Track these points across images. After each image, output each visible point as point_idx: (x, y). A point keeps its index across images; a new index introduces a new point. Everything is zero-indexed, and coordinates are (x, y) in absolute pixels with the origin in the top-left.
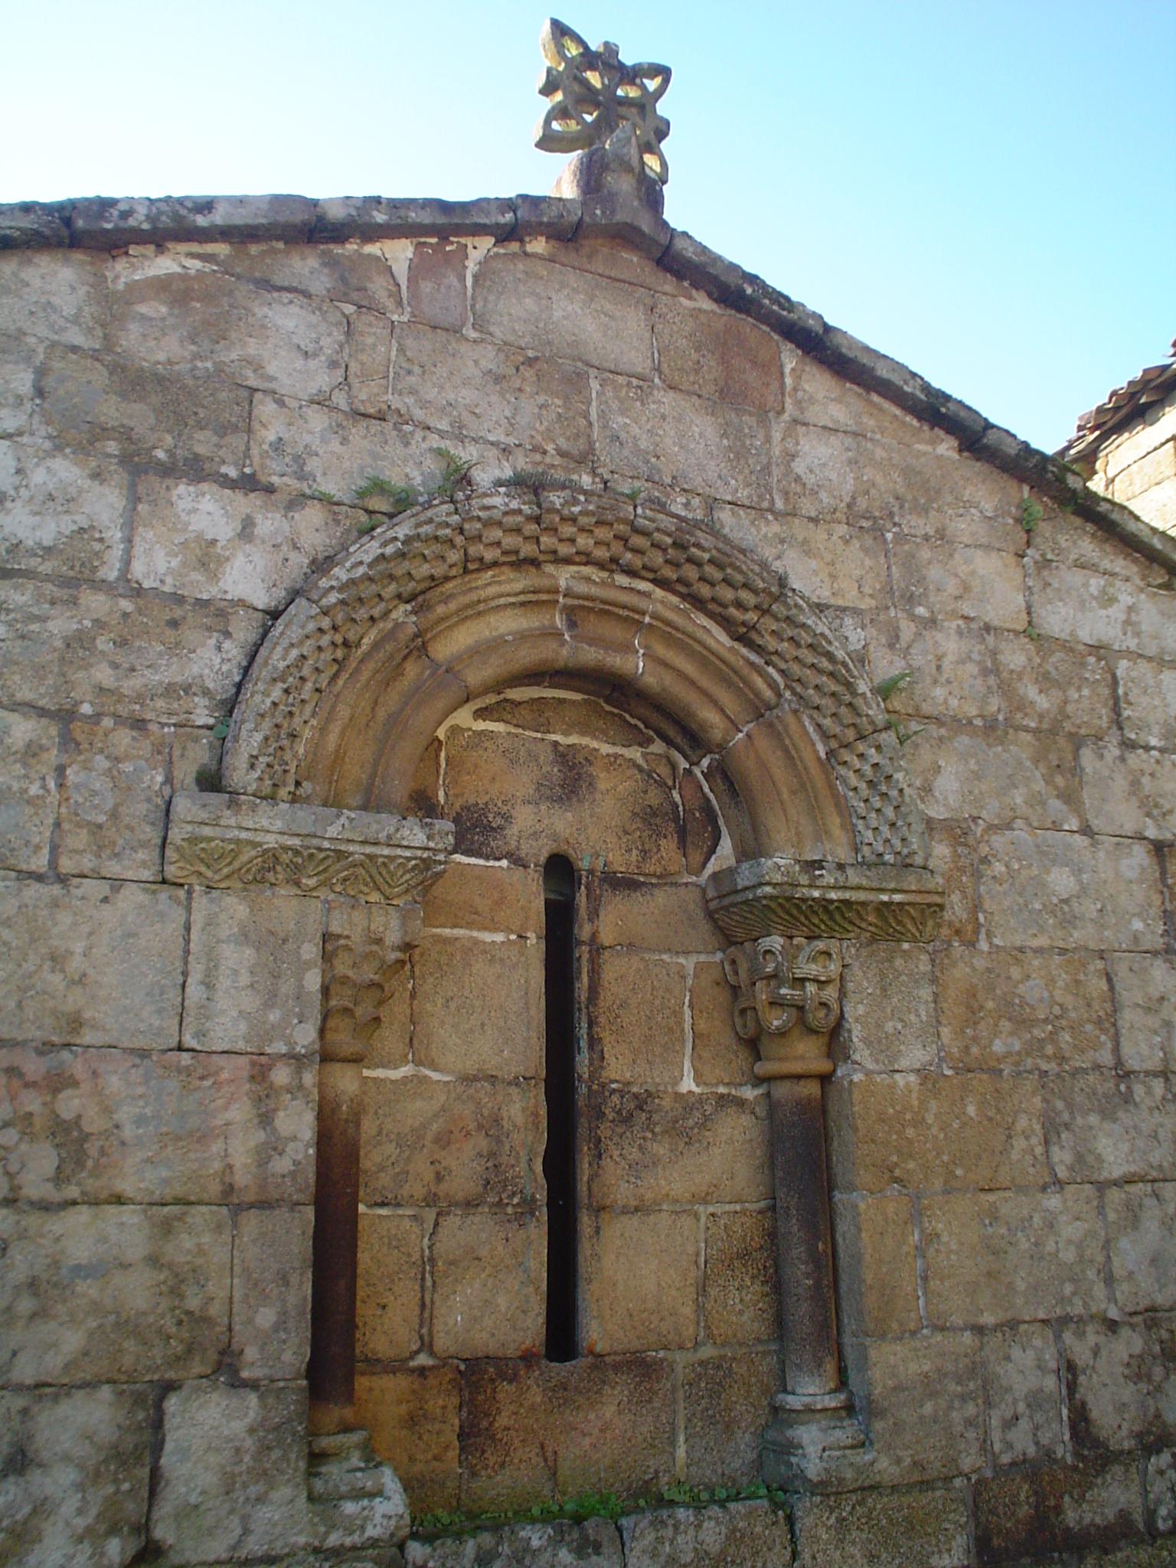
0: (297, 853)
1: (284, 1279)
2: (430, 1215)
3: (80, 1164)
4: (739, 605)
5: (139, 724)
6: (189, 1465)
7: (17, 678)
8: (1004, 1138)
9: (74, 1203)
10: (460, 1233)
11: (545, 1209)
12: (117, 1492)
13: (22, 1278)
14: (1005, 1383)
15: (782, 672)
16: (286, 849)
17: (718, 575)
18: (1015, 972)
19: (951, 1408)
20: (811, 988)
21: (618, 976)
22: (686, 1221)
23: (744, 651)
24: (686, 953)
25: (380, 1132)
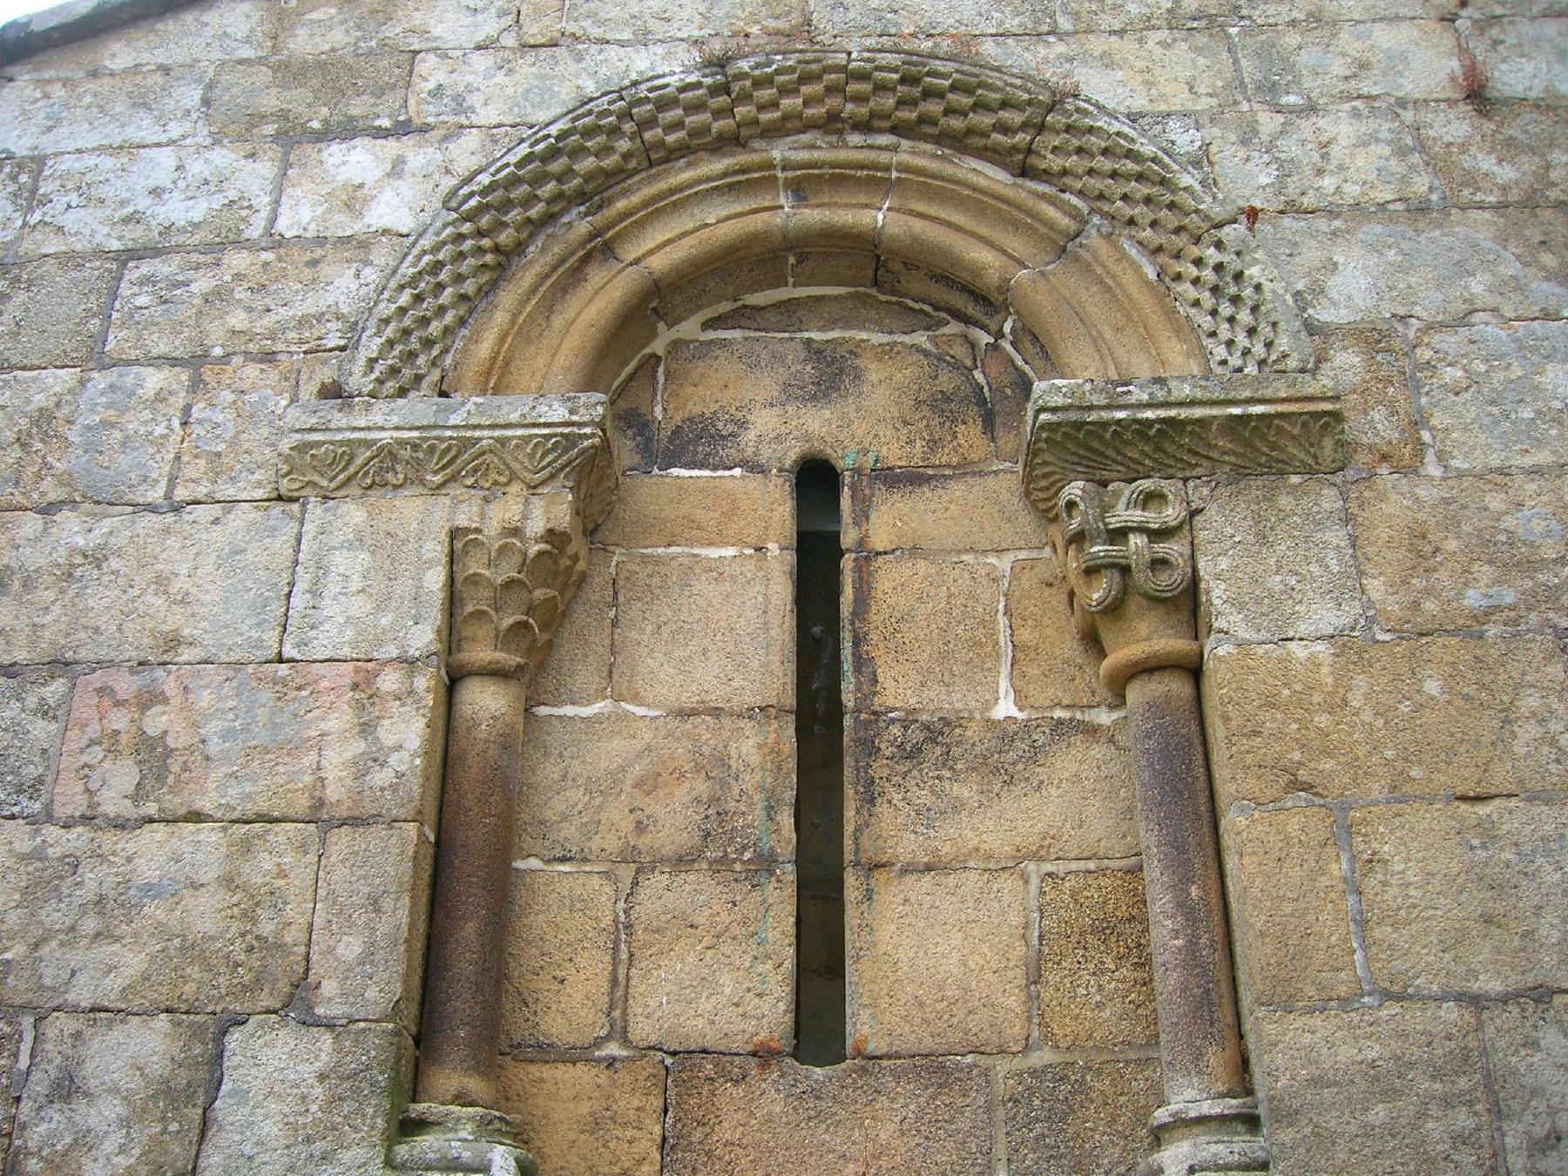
0: (415, 447)
1: (375, 904)
2: (626, 873)
3: (161, 779)
4: (1004, 129)
5: (269, 357)
6: (247, 1110)
7: (155, 337)
8: (1496, 723)
9: (151, 821)
10: (661, 895)
11: (790, 867)
12: (164, 1131)
13: (91, 896)
14: (1529, 1081)
15: (1080, 193)
16: (402, 443)
17: (967, 101)
18: (1495, 502)
19: (1422, 1115)
20: (1136, 541)
21: (894, 586)
22: (1007, 882)
23: (1032, 185)
24: (999, 551)
25: (564, 778)
